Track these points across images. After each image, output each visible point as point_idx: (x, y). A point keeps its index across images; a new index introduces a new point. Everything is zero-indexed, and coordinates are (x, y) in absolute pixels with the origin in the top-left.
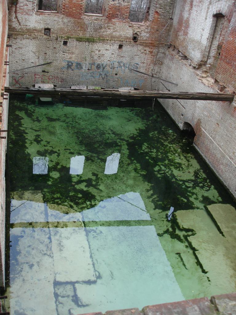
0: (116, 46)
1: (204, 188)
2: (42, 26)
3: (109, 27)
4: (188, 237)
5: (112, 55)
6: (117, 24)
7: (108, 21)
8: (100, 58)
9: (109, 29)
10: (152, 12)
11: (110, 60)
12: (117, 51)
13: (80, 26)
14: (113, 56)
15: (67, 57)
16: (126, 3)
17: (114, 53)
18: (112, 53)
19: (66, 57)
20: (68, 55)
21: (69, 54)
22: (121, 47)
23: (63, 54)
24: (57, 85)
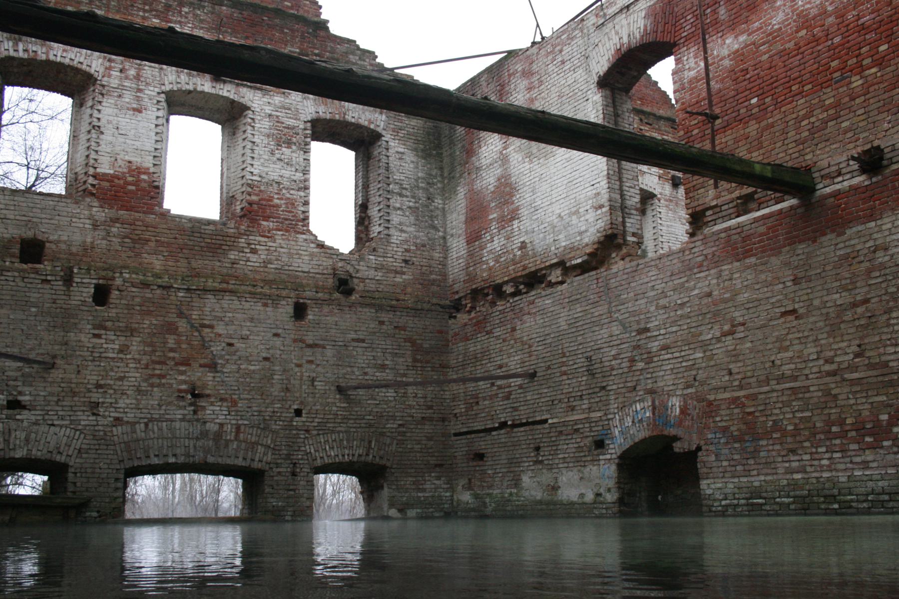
0: (286, 309)
1: (356, 573)
2: (11, 231)
3: (253, 246)
4: (64, 193)
5: (276, 339)
6: (277, 237)
7: (248, 226)
8: (232, 349)
9: (254, 251)
10: (241, 459)
11: (268, 356)
12: (290, 325)
13: (153, 239)
14: (278, 342)
15: (110, 346)
16: (297, 174)
17: (280, 331)
18: (274, 331)
19: (105, 346)
20: (113, 338)
21: (118, 333)
22: (300, 311)
23: (96, 332)
24: (71, 464)
